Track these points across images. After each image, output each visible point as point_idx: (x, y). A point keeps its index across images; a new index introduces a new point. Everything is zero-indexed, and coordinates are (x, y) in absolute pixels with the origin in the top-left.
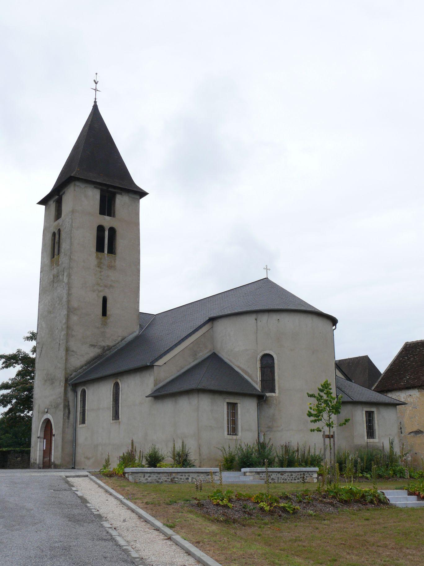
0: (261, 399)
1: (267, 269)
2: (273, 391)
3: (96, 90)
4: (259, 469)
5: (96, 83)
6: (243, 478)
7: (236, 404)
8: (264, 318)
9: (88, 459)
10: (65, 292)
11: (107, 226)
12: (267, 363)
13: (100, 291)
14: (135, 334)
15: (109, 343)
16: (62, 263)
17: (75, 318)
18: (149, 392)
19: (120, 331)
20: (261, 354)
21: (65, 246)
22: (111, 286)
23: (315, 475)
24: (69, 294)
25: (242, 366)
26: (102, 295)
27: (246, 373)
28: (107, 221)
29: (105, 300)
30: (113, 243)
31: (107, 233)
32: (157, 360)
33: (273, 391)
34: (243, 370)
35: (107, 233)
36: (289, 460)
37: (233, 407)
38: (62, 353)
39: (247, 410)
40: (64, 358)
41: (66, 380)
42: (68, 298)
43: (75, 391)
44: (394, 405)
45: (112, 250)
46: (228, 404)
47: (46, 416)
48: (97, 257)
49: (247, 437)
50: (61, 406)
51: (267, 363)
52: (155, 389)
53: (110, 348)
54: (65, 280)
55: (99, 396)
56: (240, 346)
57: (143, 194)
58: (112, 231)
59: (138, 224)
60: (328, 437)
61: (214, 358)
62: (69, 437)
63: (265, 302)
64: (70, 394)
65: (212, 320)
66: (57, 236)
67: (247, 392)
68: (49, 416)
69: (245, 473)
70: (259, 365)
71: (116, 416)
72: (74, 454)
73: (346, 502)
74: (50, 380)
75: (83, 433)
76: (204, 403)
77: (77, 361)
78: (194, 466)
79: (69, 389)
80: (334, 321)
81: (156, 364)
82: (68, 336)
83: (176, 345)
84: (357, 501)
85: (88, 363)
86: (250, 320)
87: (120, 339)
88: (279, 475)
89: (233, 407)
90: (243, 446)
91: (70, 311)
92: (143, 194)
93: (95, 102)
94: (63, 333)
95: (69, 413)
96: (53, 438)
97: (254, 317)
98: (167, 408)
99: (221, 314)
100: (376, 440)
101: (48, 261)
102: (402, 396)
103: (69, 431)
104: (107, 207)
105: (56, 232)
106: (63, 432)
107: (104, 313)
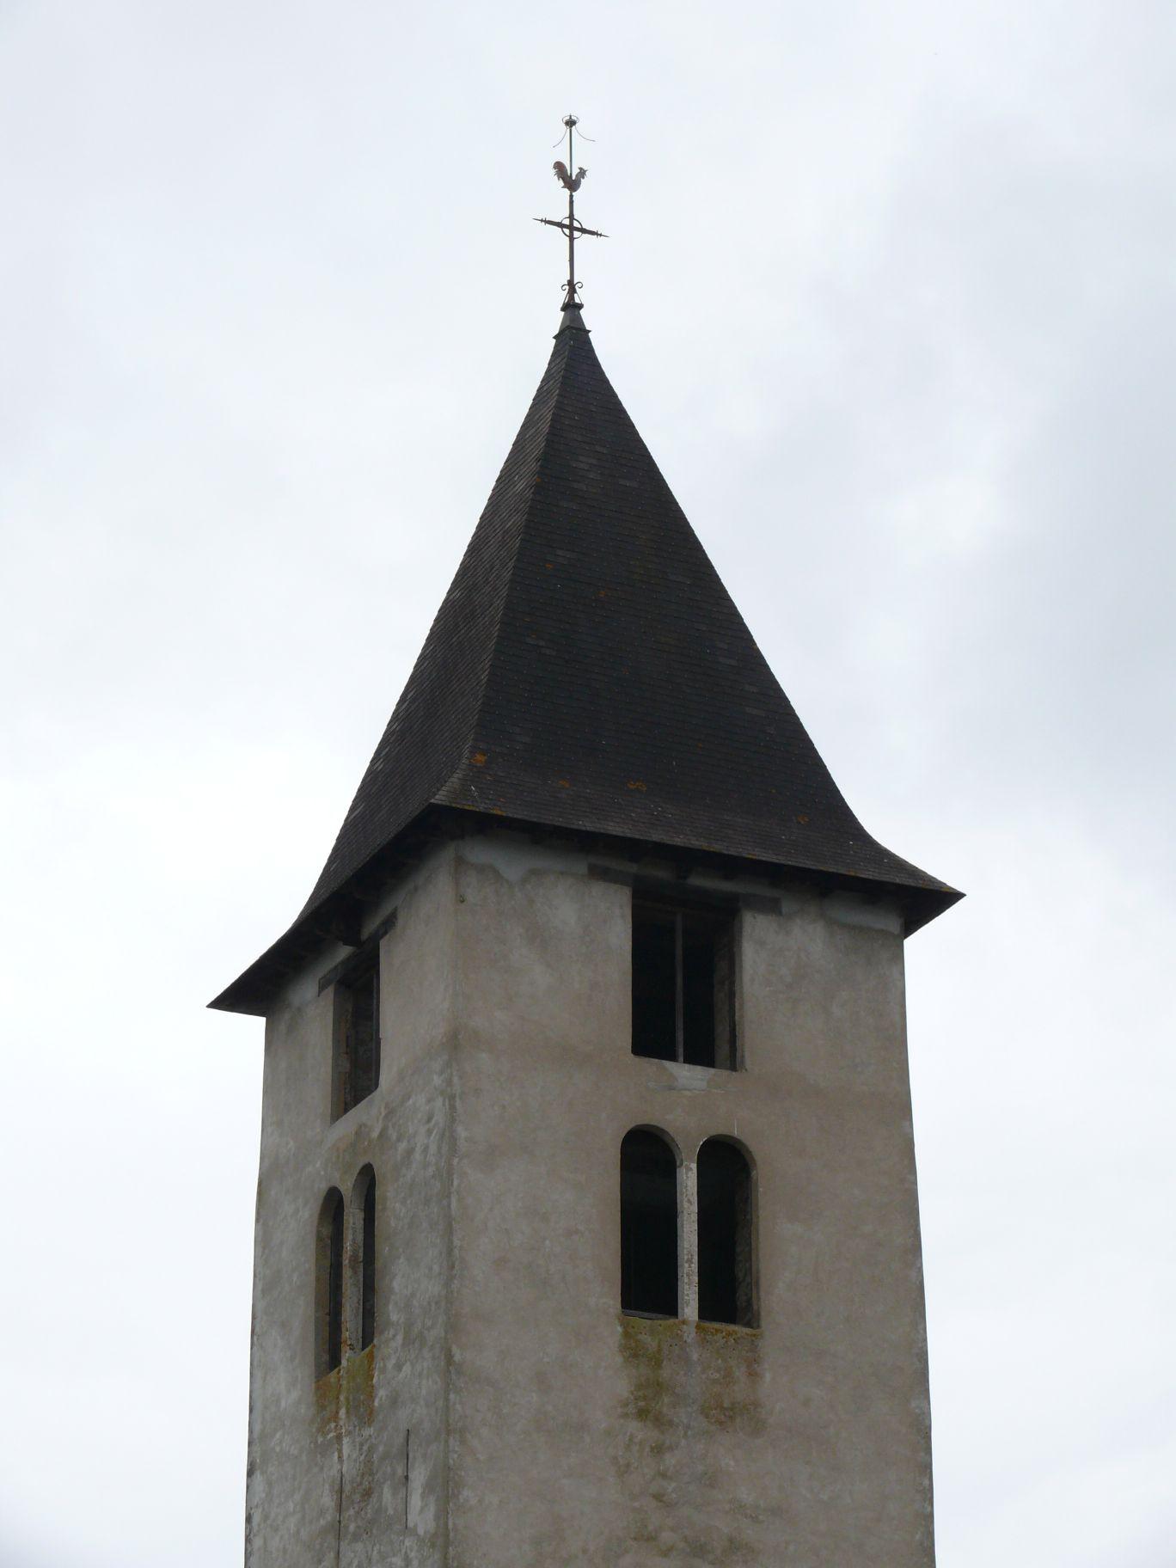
3: (571, 228)
5: (572, 184)
16: (394, 1401)
21: (408, 1282)
28: (687, 1099)
31: (688, 1180)
35: (688, 1180)
45: (729, 1298)
48: (632, 1351)
54: (421, 1515)
57: (924, 899)
58: (727, 1164)
59: (894, 1107)
92: (924, 899)
93: (572, 308)
101: (295, 1392)
104: (682, 1004)
105: (347, 1187)
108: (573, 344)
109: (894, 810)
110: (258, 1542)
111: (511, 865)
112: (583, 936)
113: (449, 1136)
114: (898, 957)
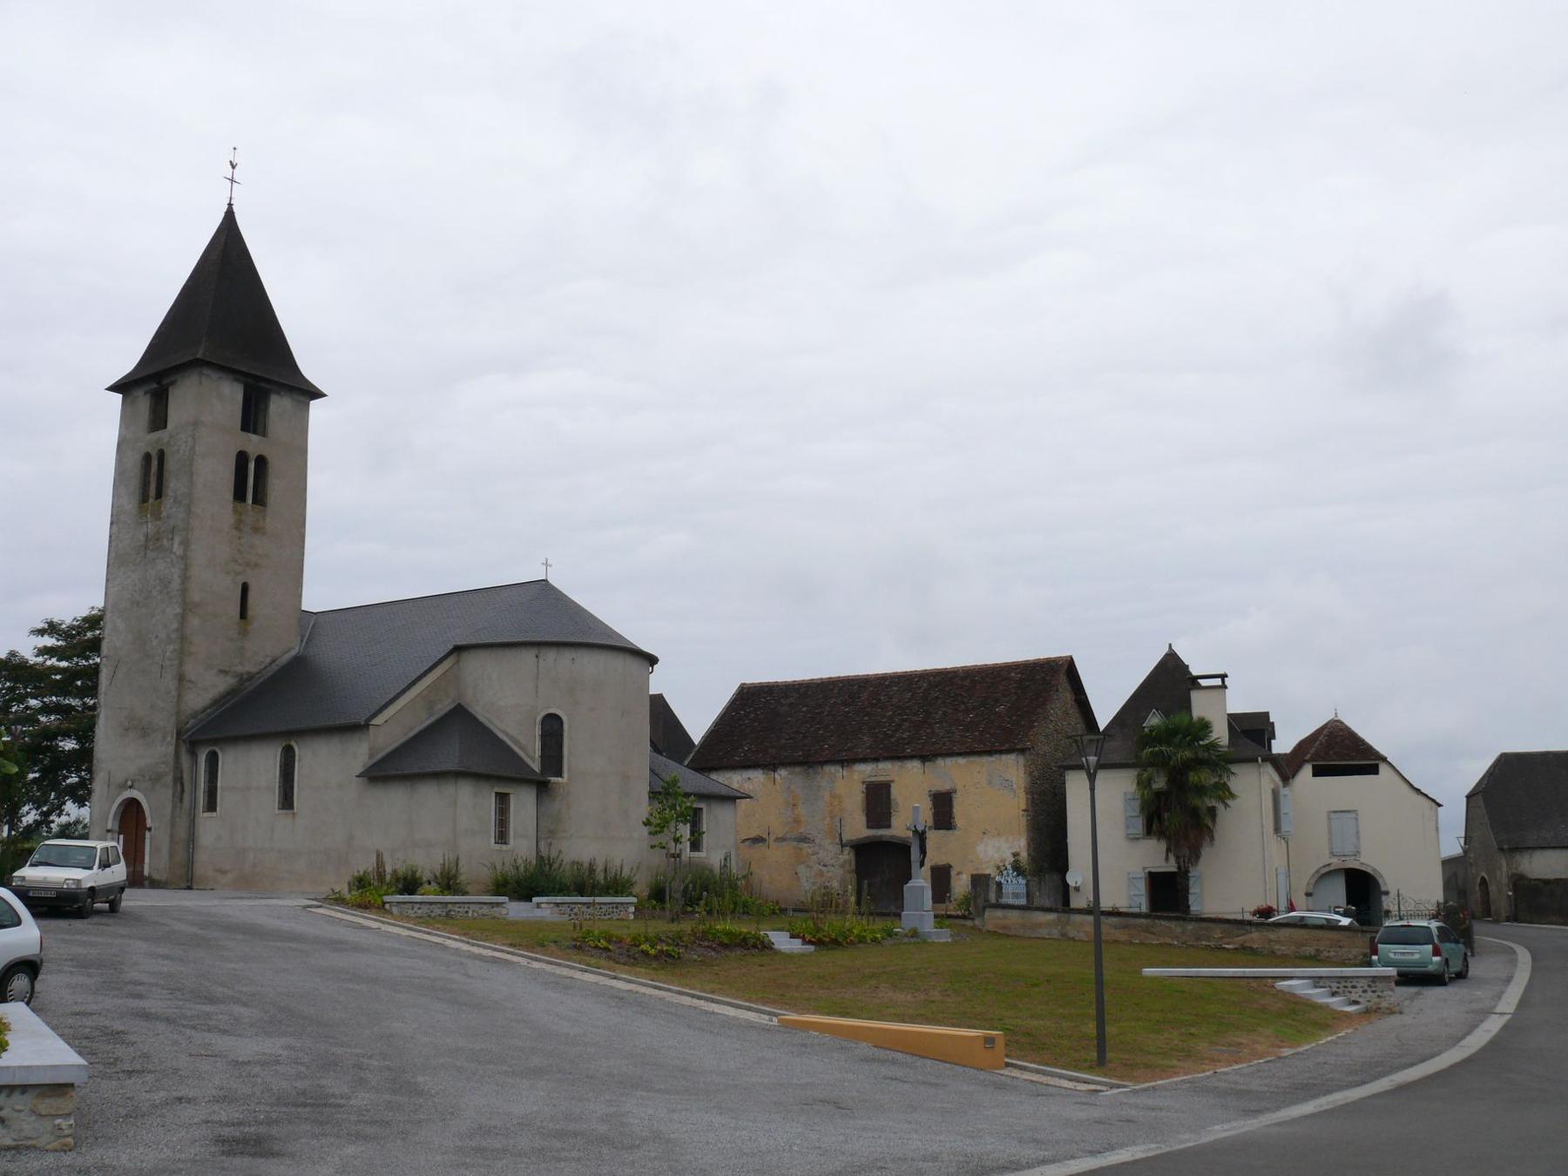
0: (542, 787)
1: (546, 564)
2: (560, 774)
3: (232, 180)
4: (559, 899)
5: (234, 167)
6: (538, 913)
7: (507, 795)
8: (550, 655)
9: (224, 872)
10: (176, 573)
11: (253, 453)
12: (552, 729)
13: (238, 574)
14: (293, 653)
15: (250, 668)
16: (168, 517)
17: (194, 622)
18: (360, 770)
19: (269, 647)
20: (543, 714)
21: (174, 485)
22: (257, 565)
23: (632, 909)
24: (185, 578)
25: (508, 730)
26: (241, 580)
27: (517, 742)
28: (254, 444)
29: (245, 588)
30: (262, 484)
31: (252, 466)
32: (375, 715)
33: (560, 774)
34: (512, 738)
35: (252, 466)
36: (585, 884)
37: (503, 799)
38: (169, 683)
39: (523, 803)
40: (174, 693)
41: (179, 734)
42: (183, 583)
43: (193, 755)
44: (730, 798)
45: (260, 500)
46: (497, 794)
47: (128, 794)
48: (235, 511)
49: (522, 848)
50: (169, 779)
51: (552, 729)
52: (371, 763)
53: (251, 677)
54: (177, 549)
55: (249, 770)
56: (507, 698)
57: (317, 394)
58: (261, 462)
59: (303, 451)
60: (673, 856)
61: (460, 716)
62: (182, 833)
63: (539, 623)
64: (185, 760)
65: (458, 649)
66: (155, 463)
67: (522, 777)
68: (135, 794)
69: (538, 905)
70: (538, 731)
71: (287, 801)
72: (190, 863)
73: (725, 946)
74: (139, 729)
75: (210, 829)
76: (465, 793)
77: (197, 700)
78: (465, 893)
79: (183, 749)
80: (652, 660)
81: (374, 722)
82: (182, 654)
83: (404, 691)
84: (738, 945)
85: (216, 702)
86: (528, 656)
87: (268, 660)
88: (584, 908)
89: (503, 799)
90: (520, 861)
91: (187, 608)
92: (317, 394)
93: (230, 205)
94: (171, 647)
95: (183, 791)
96: (148, 834)
97: (532, 652)
98: (395, 799)
99: (474, 642)
100: (702, 854)
101: (130, 504)
102: (735, 780)
103: (183, 824)
104: (253, 419)
105: (154, 454)
106: (173, 825)
107: (243, 614)
108: (230, 216)
109: (310, 366)
110: (1254, 984)
111: (214, 375)
112: (227, 397)
113: (193, 449)
114: (306, 408)
